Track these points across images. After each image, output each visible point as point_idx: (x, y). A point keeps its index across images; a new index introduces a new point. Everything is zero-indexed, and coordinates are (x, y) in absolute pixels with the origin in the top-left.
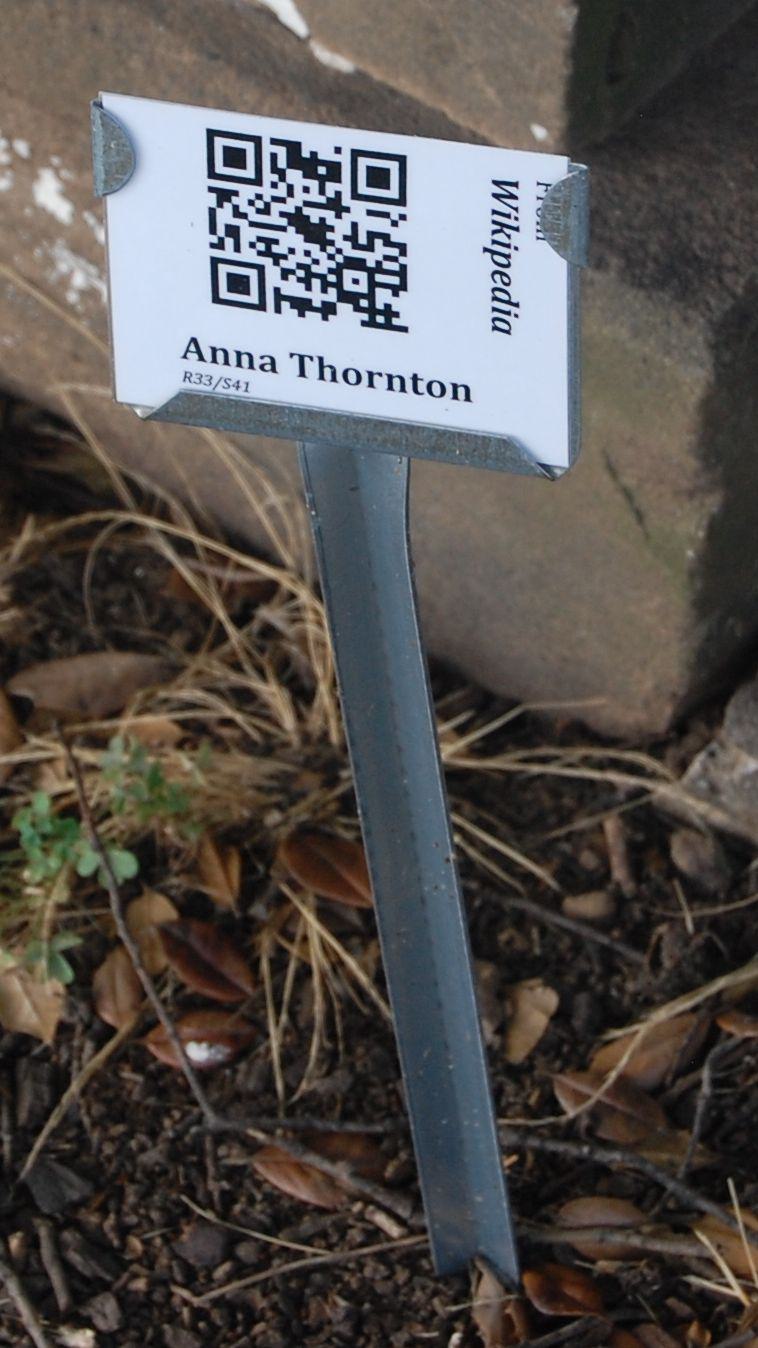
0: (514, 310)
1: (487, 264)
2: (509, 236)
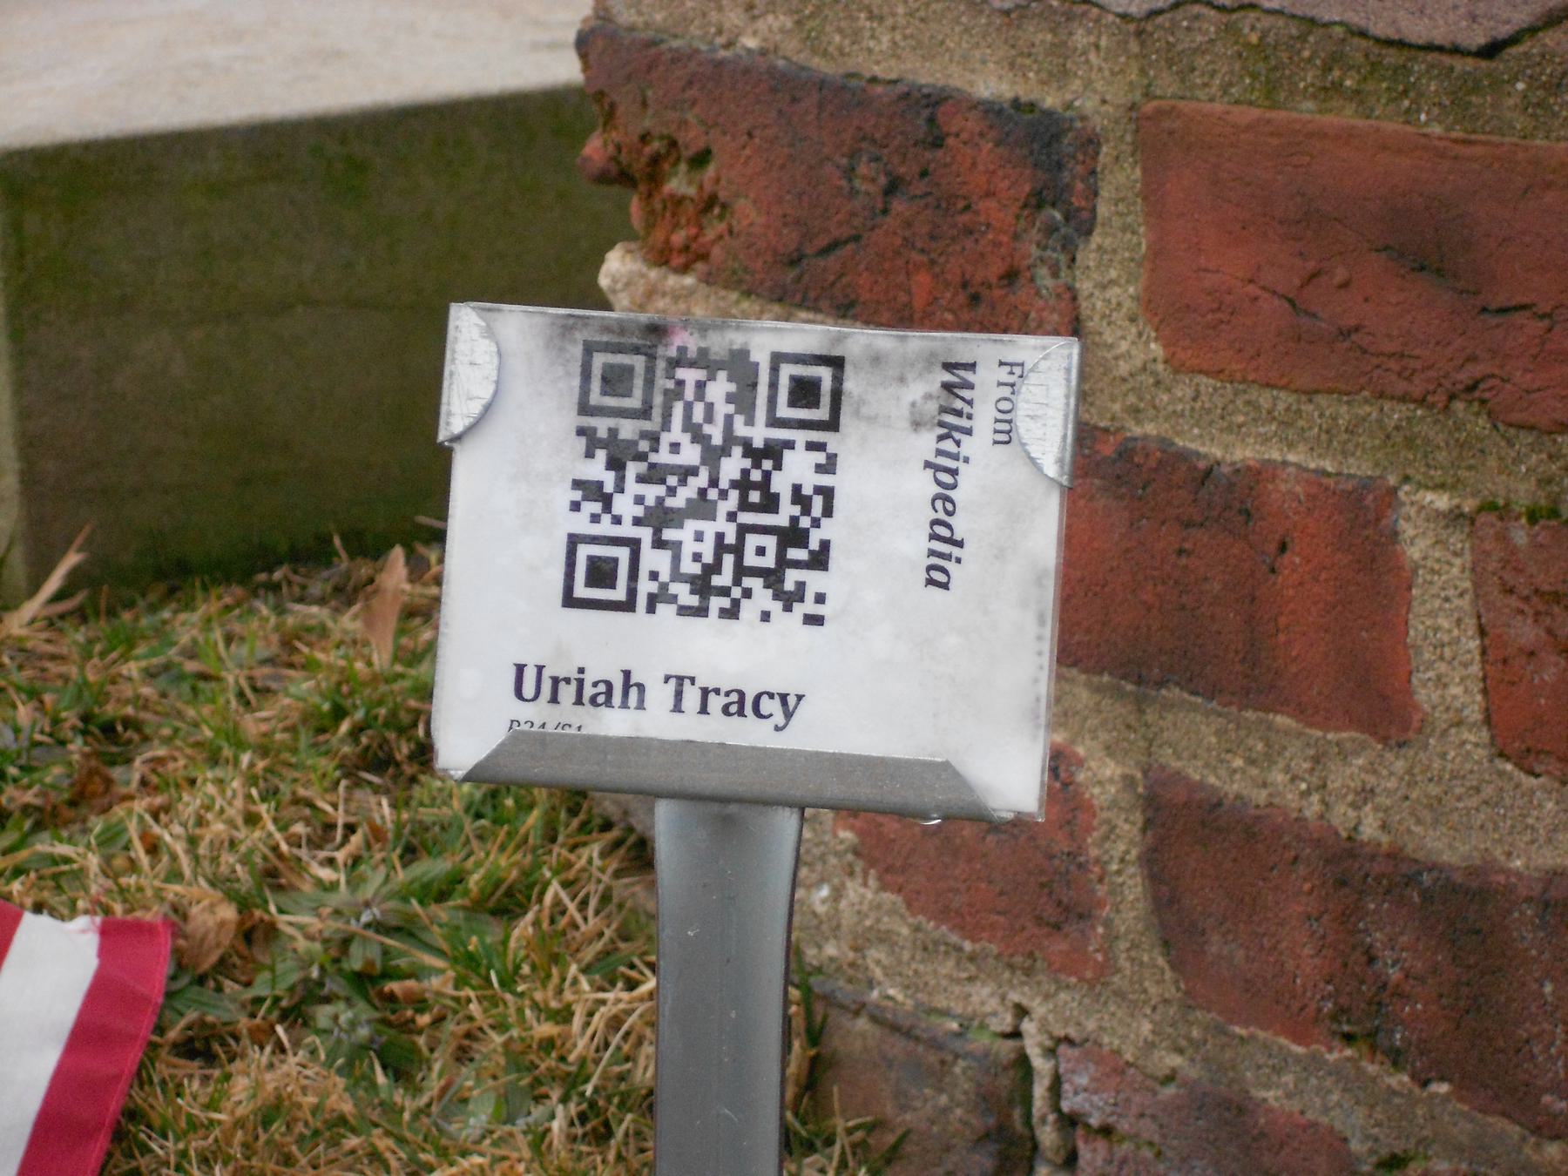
0: (956, 551)
2: (958, 443)
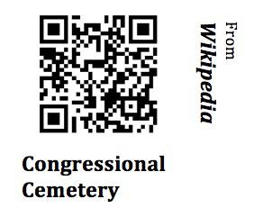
0: (213, 106)
2: (210, 59)
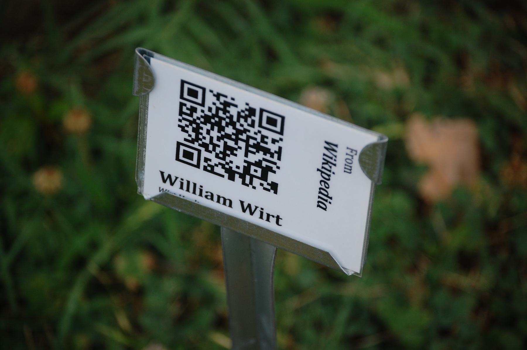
0: (329, 200)
1: (318, 177)
2: (331, 167)
